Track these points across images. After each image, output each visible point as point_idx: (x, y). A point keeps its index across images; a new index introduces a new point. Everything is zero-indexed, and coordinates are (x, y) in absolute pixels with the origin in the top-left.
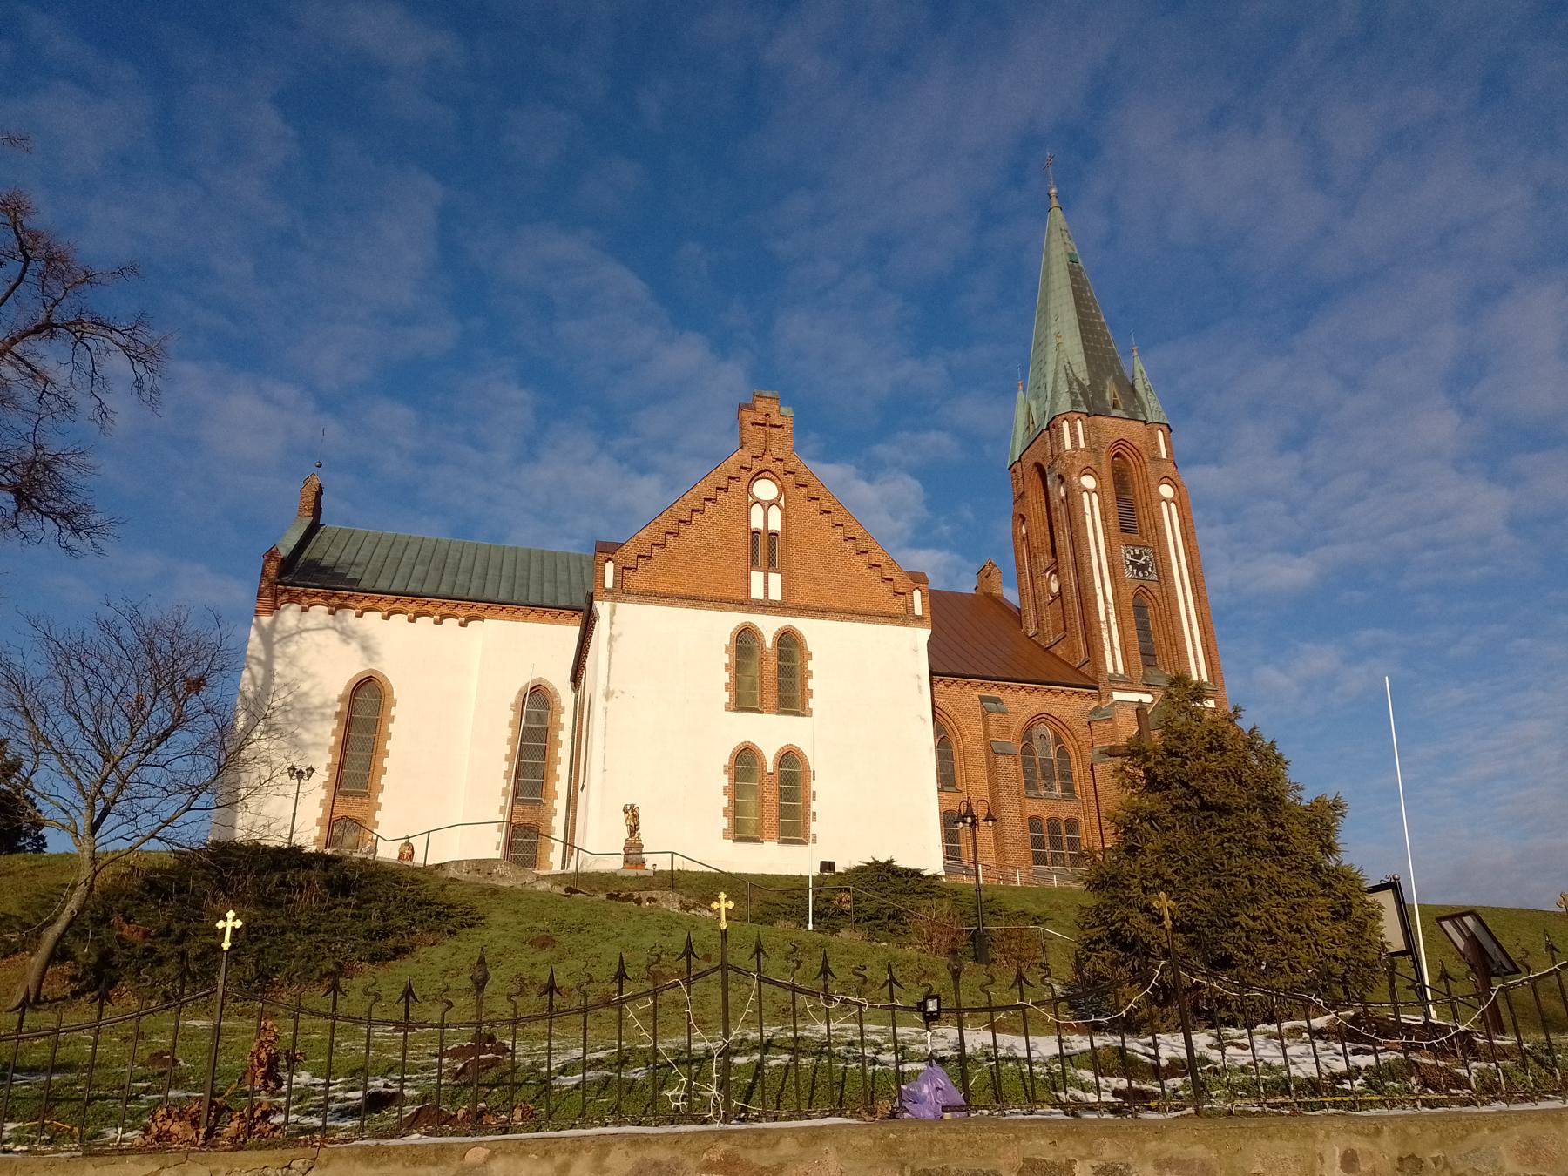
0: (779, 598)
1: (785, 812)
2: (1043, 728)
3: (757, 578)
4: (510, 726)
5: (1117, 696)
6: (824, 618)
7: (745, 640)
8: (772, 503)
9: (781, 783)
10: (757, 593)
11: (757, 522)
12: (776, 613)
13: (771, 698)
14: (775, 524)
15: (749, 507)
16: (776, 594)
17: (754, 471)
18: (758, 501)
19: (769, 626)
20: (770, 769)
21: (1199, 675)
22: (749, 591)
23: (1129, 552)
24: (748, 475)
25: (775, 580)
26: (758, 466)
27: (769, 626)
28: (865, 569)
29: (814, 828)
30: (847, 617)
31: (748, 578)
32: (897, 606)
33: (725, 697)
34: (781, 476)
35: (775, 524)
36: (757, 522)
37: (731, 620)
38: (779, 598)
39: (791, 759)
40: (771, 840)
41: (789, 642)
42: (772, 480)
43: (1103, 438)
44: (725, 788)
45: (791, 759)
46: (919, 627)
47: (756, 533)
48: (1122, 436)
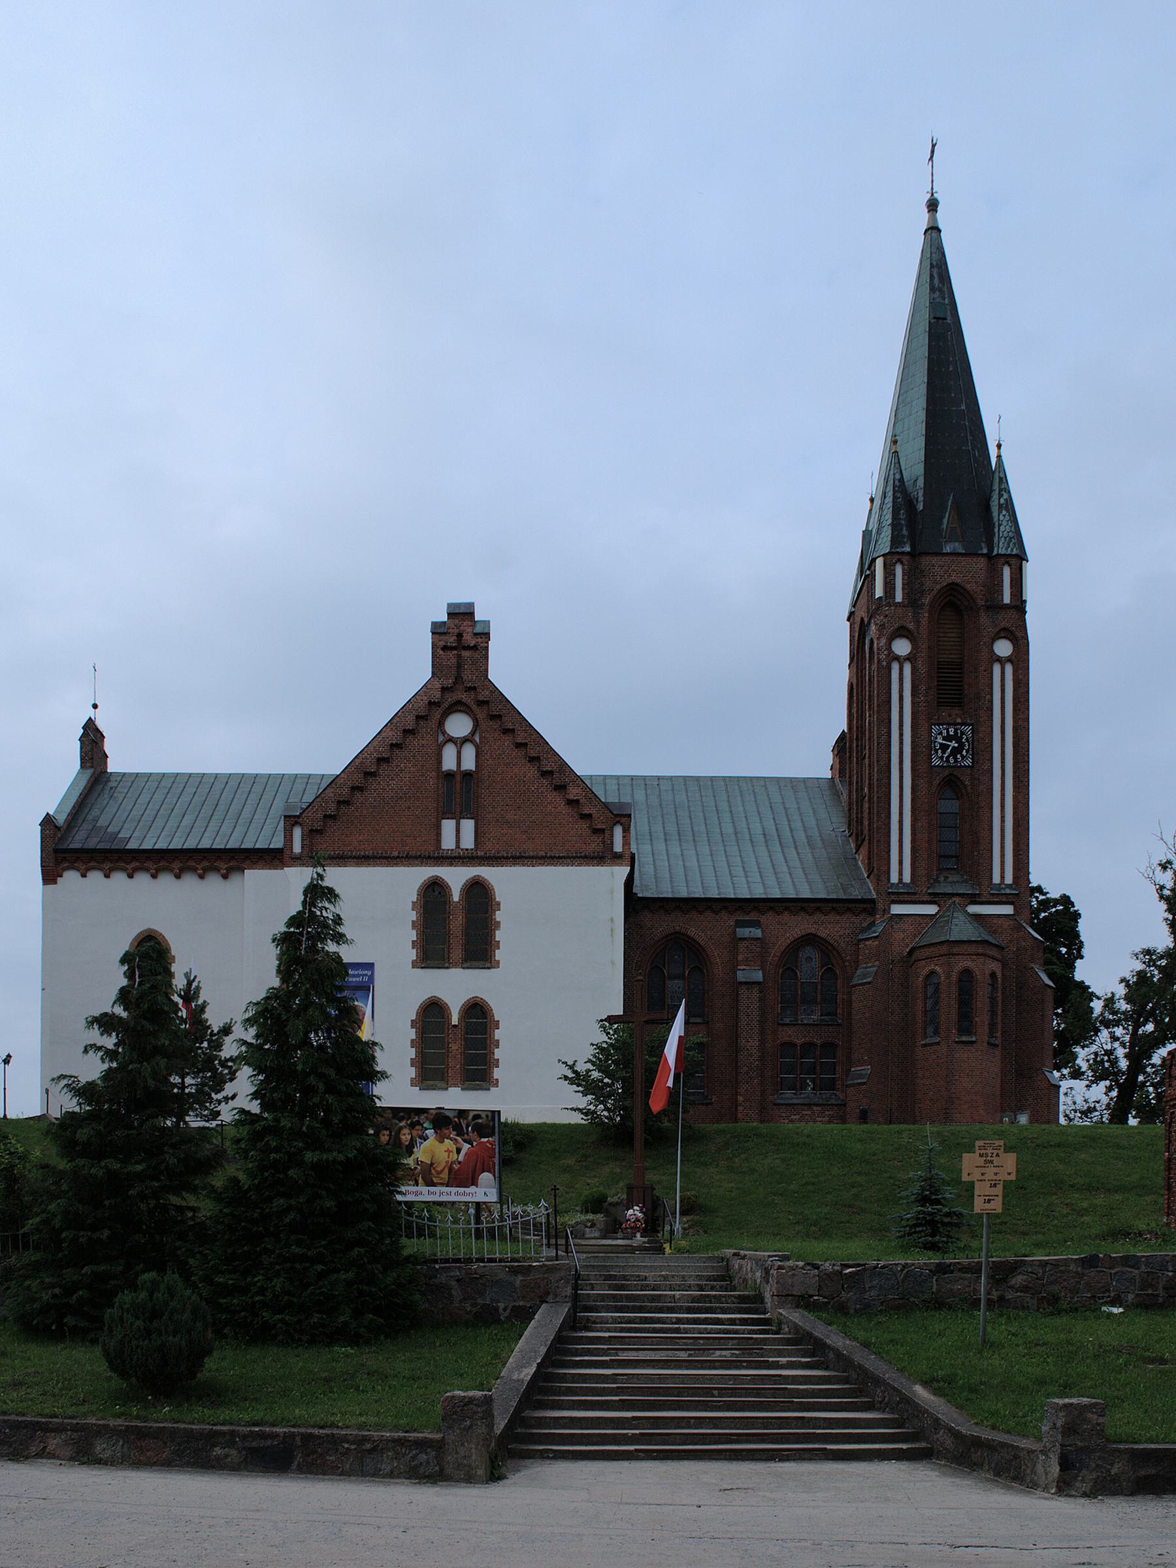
0: (1009, 602)
1: (469, 1060)
2: (809, 951)
3: (448, 826)
4: (412, 1066)
5: (897, 909)
6: (514, 865)
7: (434, 891)
8: (465, 740)
9: (467, 1033)
10: (448, 842)
11: (449, 762)
12: (464, 864)
13: (457, 953)
14: (469, 763)
15: (440, 747)
16: (468, 842)
17: (446, 705)
18: (451, 740)
19: (456, 878)
20: (455, 1020)
21: (1002, 877)
22: (439, 841)
23: (941, 733)
24: (437, 715)
25: (468, 826)
26: (451, 698)
27: (456, 878)
28: (562, 807)
29: (497, 1073)
30: (539, 861)
31: (438, 827)
32: (594, 845)
33: (413, 954)
34: (474, 707)
35: (469, 763)
36: (449, 762)
37: (417, 876)
38: (1009, 602)
39: (477, 1011)
40: (455, 1085)
41: (479, 892)
42: (468, 714)
43: (928, 584)
44: (412, 1041)
45: (477, 1011)
46: (617, 865)
47: (449, 775)
48: (954, 578)
